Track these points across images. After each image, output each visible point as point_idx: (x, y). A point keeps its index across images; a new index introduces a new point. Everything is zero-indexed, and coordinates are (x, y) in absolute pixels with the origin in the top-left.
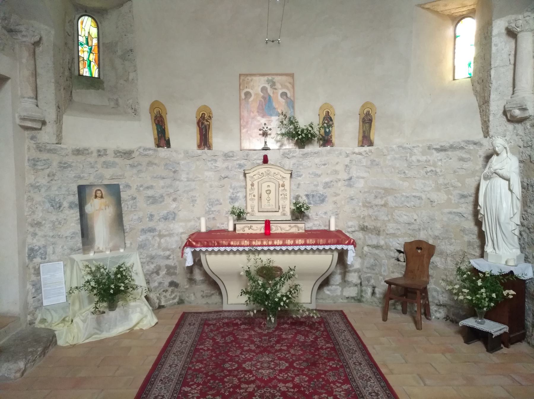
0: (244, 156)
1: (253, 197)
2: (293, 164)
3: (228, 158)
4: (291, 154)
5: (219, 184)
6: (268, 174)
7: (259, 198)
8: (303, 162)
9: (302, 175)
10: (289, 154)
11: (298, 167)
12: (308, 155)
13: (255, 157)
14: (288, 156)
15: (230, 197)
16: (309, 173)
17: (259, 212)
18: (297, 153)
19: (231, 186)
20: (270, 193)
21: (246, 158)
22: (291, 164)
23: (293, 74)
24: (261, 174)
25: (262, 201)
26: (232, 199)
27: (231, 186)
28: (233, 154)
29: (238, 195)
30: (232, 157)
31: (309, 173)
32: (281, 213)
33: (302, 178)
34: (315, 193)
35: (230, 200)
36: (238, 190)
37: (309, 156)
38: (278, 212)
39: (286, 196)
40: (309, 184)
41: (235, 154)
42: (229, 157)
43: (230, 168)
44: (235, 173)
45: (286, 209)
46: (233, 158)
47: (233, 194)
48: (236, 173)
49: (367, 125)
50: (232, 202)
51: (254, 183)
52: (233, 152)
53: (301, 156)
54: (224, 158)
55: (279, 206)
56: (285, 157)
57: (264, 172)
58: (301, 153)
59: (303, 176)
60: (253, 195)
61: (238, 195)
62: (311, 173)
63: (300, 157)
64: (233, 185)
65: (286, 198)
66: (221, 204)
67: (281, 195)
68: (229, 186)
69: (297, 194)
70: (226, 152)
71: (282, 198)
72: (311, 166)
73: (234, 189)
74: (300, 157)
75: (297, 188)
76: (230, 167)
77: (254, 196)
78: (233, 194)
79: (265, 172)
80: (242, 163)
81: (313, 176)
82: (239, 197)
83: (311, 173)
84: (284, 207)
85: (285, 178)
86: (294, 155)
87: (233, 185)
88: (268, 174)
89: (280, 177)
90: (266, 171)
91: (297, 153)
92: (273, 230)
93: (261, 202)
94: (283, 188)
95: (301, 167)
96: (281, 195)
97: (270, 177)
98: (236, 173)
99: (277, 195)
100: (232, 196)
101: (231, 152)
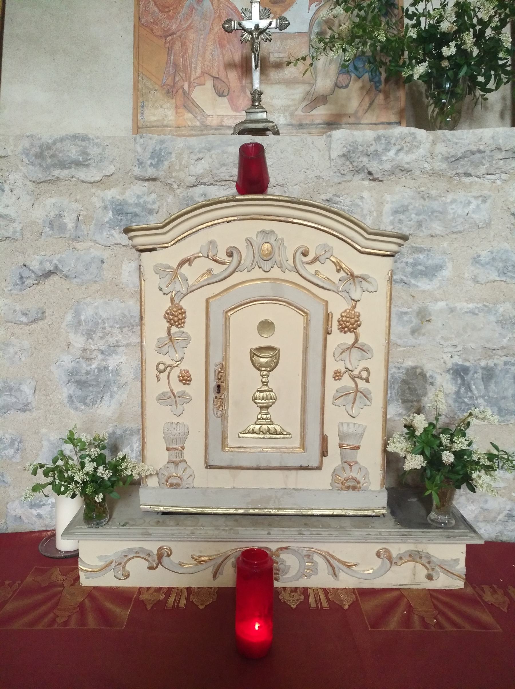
0: (141, 163)
1: (178, 387)
2: (396, 212)
3: (57, 172)
4: (391, 154)
5: (18, 307)
6: (268, 257)
7: (212, 395)
8: (450, 197)
9: (439, 268)
10: (376, 154)
11: (420, 224)
12: (476, 165)
13: (199, 168)
14: (374, 166)
15: (73, 373)
16: (476, 260)
17: (208, 466)
18: (422, 151)
19: (77, 314)
20: (272, 367)
21: (151, 172)
22: (387, 208)
23: (206, 468)
24: (222, 256)
25: (231, 409)
26: (81, 384)
27: (77, 314)
28: (84, 153)
29: (112, 362)
30: (78, 164)
31: (476, 260)
32: (335, 474)
33: (436, 282)
34: (499, 361)
35: (72, 389)
36: (112, 340)
37: (482, 170)
38: (319, 468)
39: (362, 384)
40: (473, 313)
41: (93, 151)
42: (63, 165)
43: (70, 225)
44: (96, 252)
45: (361, 457)
46: (82, 174)
47: (89, 360)
48: (106, 254)
49: (21, 406)
50: (83, 400)
51: (184, 304)
52: (85, 138)
53: (440, 165)
54: (38, 173)
55: (324, 440)
56: (357, 171)
57: (242, 247)
58: (441, 148)
59: (446, 273)
60: (176, 372)
61: (112, 362)
62: (485, 256)
63: (435, 174)
64: (87, 314)
65: (366, 396)
66: (25, 408)
67: (338, 376)
68: (69, 318)
69: (409, 363)
70: (46, 137)
71: (341, 394)
72: (488, 224)
73: (90, 334)
74: (435, 174)
75: (413, 332)
76: (69, 221)
77: (185, 379)
78: (89, 360)
79: (249, 242)
80: (132, 200)
81: (494, 276)
82: (117, 371)
83: (485, 256)
84: (352, 442)
85: (363, 278)
86: (405, 159)
87: (87, 314)
88: (268, 257)
89: (336, 277)
90: (257, 240)
91: (422, 151)
92: (292, 573)
93: (224, 417)
94: (349, 338)
95: (437, 227)
96: (338, 376)
97: (276, 272)
98: (106, 254)
99: (314, 377)
100: (84, 366)
101: (75, 137)
